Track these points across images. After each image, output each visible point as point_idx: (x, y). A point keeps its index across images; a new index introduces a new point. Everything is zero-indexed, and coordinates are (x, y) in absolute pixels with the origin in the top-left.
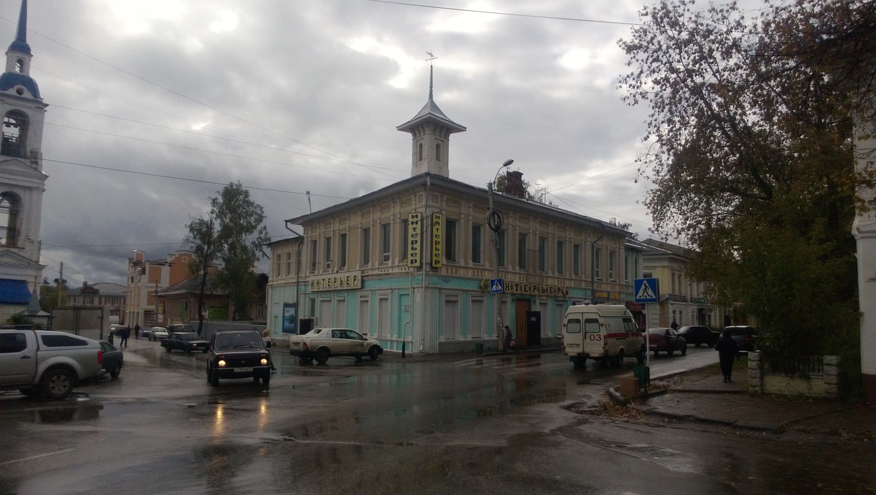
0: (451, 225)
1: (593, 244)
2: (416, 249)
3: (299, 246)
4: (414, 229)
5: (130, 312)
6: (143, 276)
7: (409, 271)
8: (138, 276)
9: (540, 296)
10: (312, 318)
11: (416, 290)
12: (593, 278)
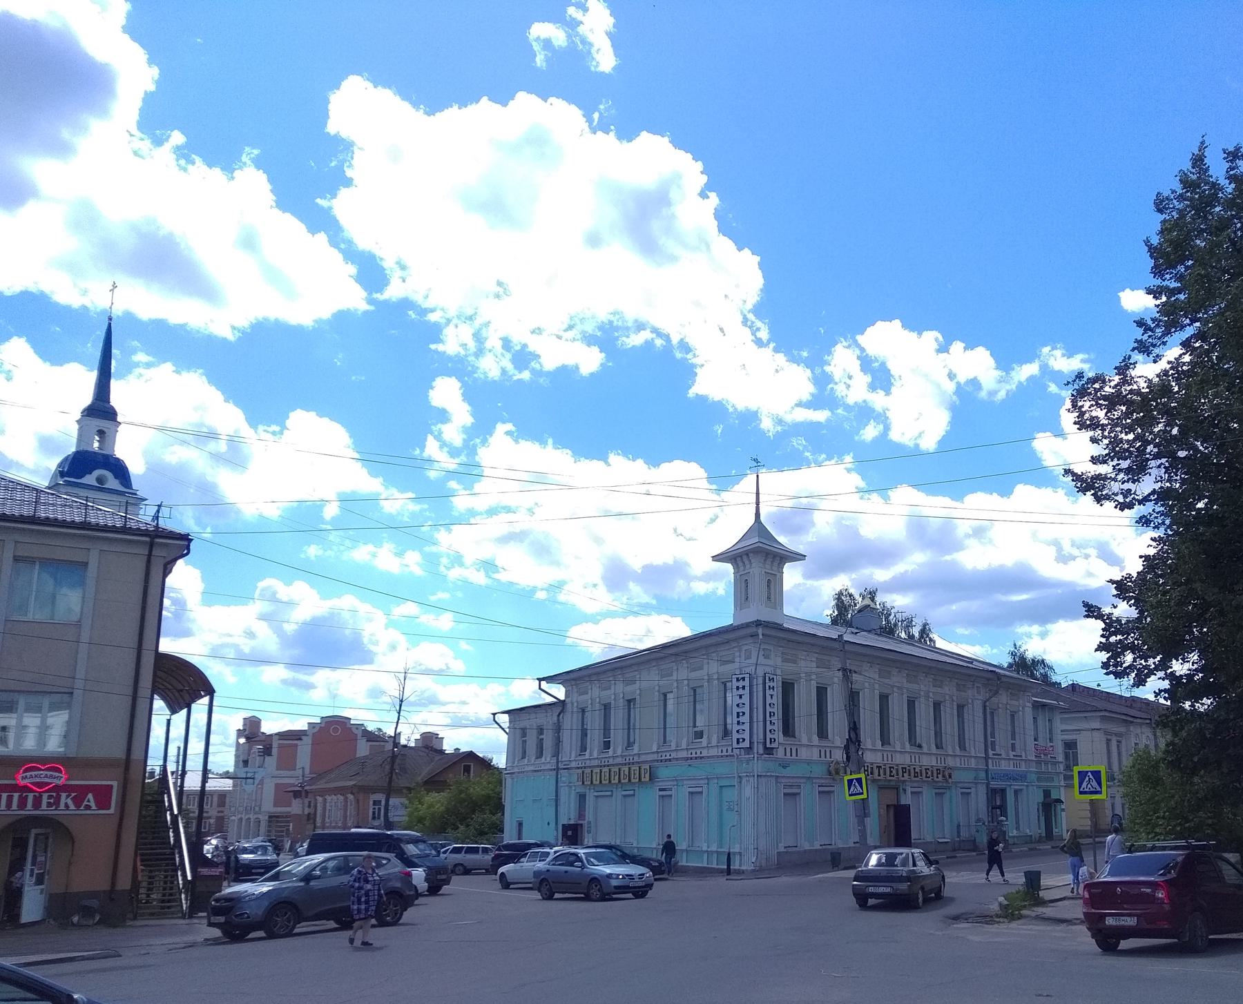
0: (788, 688)
1: (985, 702)
2: (743, 723)
3: (559, 714)
4: (741, 697)
5: (241, 819)
6: (267, 758)
7: (734, 753)
8: (258, 758)
9: (911, 781)
10: (581, 822)
11: (744, 780)
12: (986, 750)
